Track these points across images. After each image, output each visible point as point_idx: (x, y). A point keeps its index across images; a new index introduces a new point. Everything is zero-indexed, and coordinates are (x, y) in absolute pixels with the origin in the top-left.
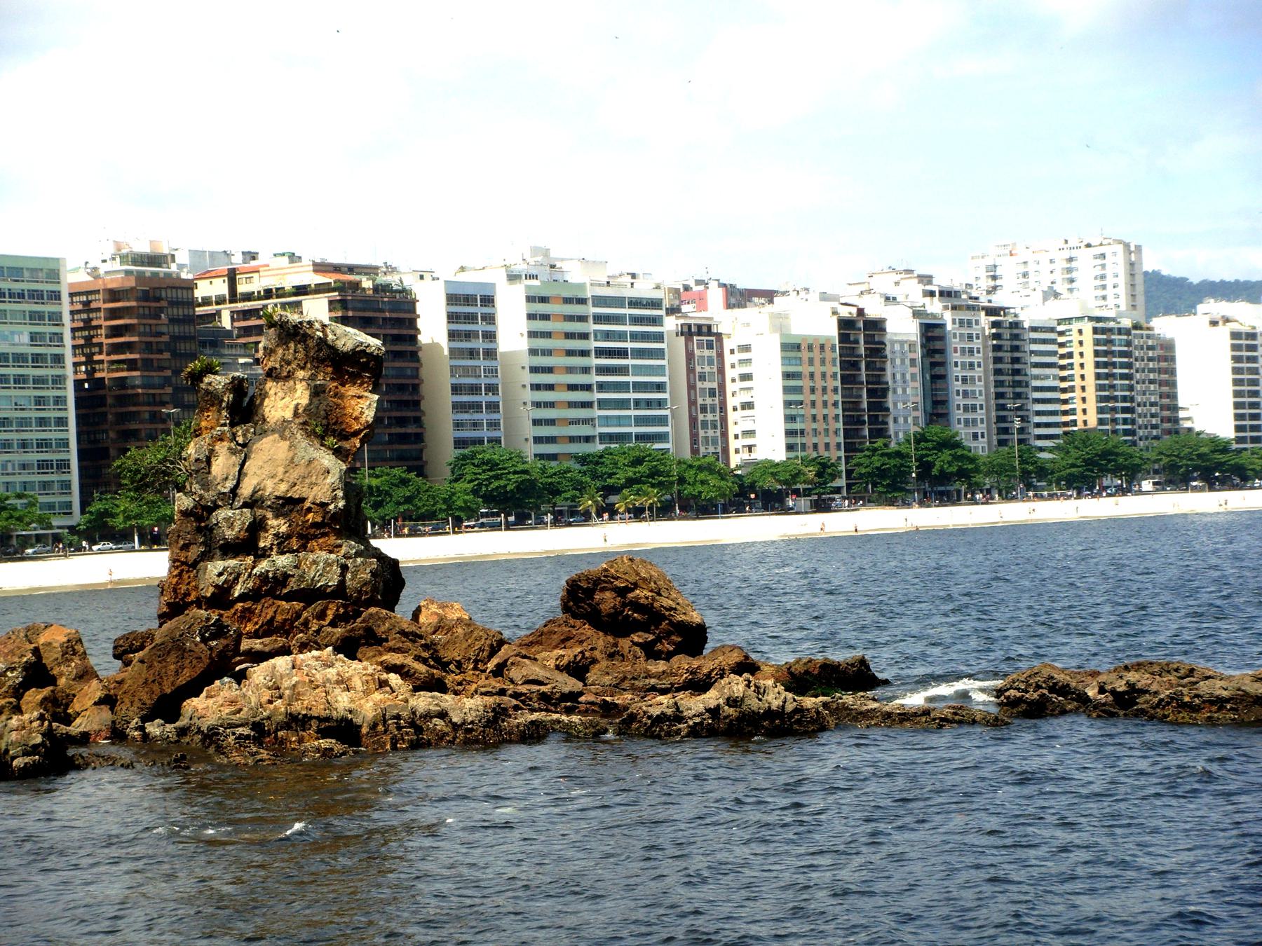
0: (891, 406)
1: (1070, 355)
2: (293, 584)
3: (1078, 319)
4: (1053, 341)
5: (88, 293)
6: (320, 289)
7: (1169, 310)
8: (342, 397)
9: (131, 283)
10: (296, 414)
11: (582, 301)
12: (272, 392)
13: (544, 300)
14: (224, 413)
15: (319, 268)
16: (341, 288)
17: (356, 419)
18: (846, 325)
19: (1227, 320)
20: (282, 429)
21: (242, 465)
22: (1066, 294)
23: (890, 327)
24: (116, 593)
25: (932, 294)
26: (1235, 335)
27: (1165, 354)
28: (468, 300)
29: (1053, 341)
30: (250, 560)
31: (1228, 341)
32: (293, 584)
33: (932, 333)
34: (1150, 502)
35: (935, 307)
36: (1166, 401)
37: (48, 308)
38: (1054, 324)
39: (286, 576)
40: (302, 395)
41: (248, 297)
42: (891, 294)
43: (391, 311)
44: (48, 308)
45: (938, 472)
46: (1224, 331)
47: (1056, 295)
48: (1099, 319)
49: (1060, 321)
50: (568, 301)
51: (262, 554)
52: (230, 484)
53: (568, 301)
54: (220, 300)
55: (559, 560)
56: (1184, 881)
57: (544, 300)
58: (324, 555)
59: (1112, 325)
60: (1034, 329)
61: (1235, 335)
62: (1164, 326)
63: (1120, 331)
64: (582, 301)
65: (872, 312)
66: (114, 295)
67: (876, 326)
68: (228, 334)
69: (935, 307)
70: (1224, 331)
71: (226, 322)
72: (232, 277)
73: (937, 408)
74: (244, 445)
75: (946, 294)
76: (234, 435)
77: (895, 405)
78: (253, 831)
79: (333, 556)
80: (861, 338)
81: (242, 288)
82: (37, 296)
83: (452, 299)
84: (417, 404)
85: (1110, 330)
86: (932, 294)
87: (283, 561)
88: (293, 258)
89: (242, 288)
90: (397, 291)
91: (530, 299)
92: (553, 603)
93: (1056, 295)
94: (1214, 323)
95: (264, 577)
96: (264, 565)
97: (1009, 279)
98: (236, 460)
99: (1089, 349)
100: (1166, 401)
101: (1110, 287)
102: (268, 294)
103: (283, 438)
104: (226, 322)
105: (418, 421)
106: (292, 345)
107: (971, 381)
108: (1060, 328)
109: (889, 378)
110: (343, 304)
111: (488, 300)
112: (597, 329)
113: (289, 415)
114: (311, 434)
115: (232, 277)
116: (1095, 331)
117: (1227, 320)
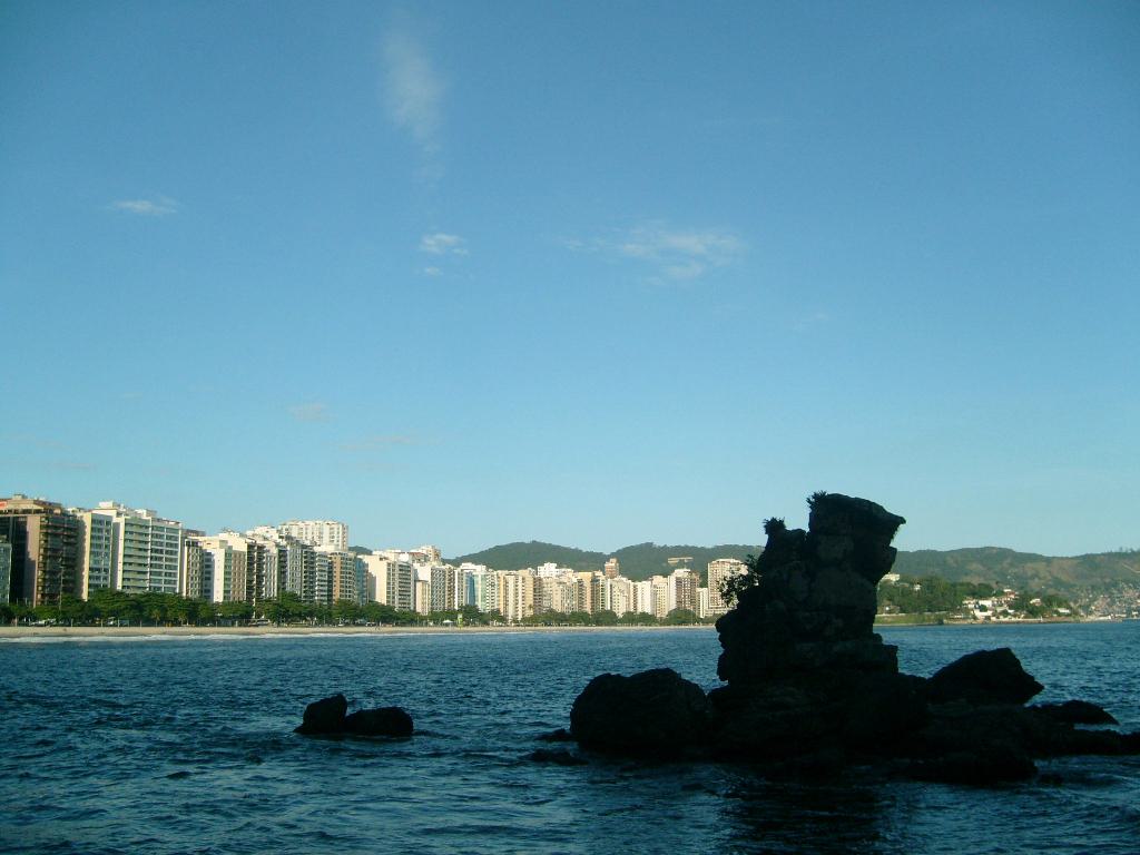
6: (38, 512)
13: (132, 525)
15: (37, 502)
18: (250, 547)
26: (389, 564)
28: (101, 522)
31: (386, 568)
33: (282, 553)
34: (366, 632)
35: (284, 543)
45: (286, 611)
50: (141, 526)
56: (491, 718)
65: (260, 542)
67: (261, 548)
69: (284, 543)
70: (385, 562)
78: (1015, 616)
80: (255, 552)
88: (24, 497)
92: (559, 713)
94: (381, 559)
107: (294, 566)
112: (155, 540)
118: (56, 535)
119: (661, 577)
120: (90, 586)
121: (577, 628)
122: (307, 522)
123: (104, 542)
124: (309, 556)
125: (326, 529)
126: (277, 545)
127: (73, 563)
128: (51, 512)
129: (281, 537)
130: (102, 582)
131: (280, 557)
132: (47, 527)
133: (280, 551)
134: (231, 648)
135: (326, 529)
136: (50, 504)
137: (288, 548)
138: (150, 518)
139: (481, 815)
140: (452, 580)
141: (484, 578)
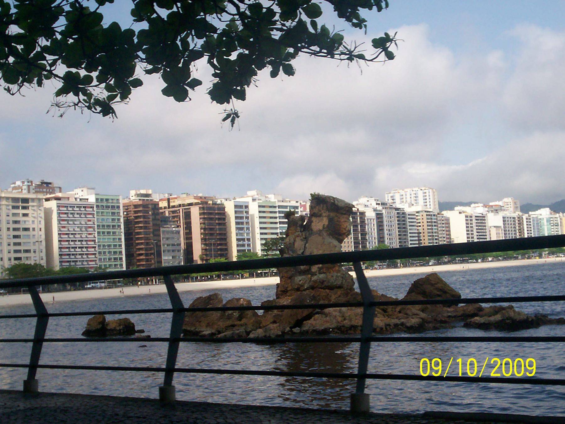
0: (367, 238)
1: (420, 223)
2: (325, 284)
3: (422, 211)
4: (415, 218)
5: (127, 206)
6: (196, 204)
7: (446, 209)
8: (340, 222)
9: (141, 203)
10: (324, 228)
11: (275, 207)
12: (314, 221)
13: (264, 207)
14: (298, 228)
16: (202, 203)
17: (345, 229)
19: (464, 212)
20: (320, 232)
21: (305, 245)
22: (415, 204)
23: (367, 214)
24: (267, 288)
25: (379, 204)
26: (466, 216)
27: (447, 222)
28: (241, 207)
29: (415, 218)
30: (310, 276)
31: (464, 218)
32: (325, 284)
33: (379, 216)
35: (380, 208)
36: (448, 236)
37: (116, 211)
38: (415, 213)
39: (324, 281)
40: (325, 221)
41: (174, 207)
42: (366, 204)
43: (218, 210)
44: (116, 211)
46: (463, 215)
47: (413, 205)
48: (428, 212)
49: (417, 212)
50: (271, 207)
51: (313, 274)
52: (302, 251)
53: (271, 207)
54: (165, 208)
55: (414, 275)
57: (264, 207)
58: (335, 274)
59: (431, 213)
60: (409, 215)
61: (466, 216)
62: (446, 213)
63: (434, 215)
64: (275, 207)
66: (136, 206)
68: (169, 217)
69: (380, 208)
70: (463, 215)
71: (167, 214)
72: (169, 200)
73: (381, 239)
74: (305, 238)
75: (383, 204)
76: (302, 235)
77: (369, 238)
79: (339, 274)
81: (171, 204)
82: (113, 207)
83: (236, 206)
84: (225, 239)
85: (431, 215)
86: (379, 204)
87: (322, 276)
89: (171, 204)
90: (219, 204)
91: (259, 206)
93: (413, 205)
94: (460, 213)
95: (315, 282)
96: (314, 278)
97: (398, 200)
98: (303, 243)
99: (425, 221)
100: (448, 236)
101: (428, 202)
102: (180, 206)
103: (320, 235)
104: (167, 214)
105: (226, 244)
106: (322, 205)
108: (417, 214)
109: (367, 230)
110: (203, 208)
111: (247, 207)
113: (321, 228)
114: (330, 235)
115: (169, 200)
116: (427, 215)
117: (464, 212)
118: (211, 219)
119: (313, 224)
120: (238, 251)
121: (536, 261)
122: (406, 190)
123: (245, 220)
124: (402, 216)
125: (420, 194)
126: (375, 210)
127: (224, 238)
128: (207, 203)
129: (377, 204)
130: (246, 248)
131: (378, 218)
132: (204, 214)
133: (377, 214)
134: (539, 273)
135: (420, 194)
136: (205, 198)
137: (384, 211)
138: (276, 200)
139: (459, 407)
140: (521, 224)
141: (548, 221)
